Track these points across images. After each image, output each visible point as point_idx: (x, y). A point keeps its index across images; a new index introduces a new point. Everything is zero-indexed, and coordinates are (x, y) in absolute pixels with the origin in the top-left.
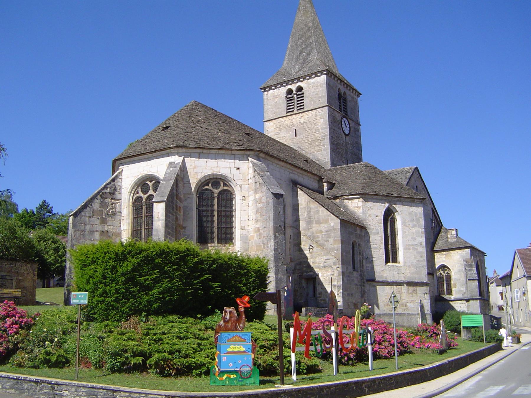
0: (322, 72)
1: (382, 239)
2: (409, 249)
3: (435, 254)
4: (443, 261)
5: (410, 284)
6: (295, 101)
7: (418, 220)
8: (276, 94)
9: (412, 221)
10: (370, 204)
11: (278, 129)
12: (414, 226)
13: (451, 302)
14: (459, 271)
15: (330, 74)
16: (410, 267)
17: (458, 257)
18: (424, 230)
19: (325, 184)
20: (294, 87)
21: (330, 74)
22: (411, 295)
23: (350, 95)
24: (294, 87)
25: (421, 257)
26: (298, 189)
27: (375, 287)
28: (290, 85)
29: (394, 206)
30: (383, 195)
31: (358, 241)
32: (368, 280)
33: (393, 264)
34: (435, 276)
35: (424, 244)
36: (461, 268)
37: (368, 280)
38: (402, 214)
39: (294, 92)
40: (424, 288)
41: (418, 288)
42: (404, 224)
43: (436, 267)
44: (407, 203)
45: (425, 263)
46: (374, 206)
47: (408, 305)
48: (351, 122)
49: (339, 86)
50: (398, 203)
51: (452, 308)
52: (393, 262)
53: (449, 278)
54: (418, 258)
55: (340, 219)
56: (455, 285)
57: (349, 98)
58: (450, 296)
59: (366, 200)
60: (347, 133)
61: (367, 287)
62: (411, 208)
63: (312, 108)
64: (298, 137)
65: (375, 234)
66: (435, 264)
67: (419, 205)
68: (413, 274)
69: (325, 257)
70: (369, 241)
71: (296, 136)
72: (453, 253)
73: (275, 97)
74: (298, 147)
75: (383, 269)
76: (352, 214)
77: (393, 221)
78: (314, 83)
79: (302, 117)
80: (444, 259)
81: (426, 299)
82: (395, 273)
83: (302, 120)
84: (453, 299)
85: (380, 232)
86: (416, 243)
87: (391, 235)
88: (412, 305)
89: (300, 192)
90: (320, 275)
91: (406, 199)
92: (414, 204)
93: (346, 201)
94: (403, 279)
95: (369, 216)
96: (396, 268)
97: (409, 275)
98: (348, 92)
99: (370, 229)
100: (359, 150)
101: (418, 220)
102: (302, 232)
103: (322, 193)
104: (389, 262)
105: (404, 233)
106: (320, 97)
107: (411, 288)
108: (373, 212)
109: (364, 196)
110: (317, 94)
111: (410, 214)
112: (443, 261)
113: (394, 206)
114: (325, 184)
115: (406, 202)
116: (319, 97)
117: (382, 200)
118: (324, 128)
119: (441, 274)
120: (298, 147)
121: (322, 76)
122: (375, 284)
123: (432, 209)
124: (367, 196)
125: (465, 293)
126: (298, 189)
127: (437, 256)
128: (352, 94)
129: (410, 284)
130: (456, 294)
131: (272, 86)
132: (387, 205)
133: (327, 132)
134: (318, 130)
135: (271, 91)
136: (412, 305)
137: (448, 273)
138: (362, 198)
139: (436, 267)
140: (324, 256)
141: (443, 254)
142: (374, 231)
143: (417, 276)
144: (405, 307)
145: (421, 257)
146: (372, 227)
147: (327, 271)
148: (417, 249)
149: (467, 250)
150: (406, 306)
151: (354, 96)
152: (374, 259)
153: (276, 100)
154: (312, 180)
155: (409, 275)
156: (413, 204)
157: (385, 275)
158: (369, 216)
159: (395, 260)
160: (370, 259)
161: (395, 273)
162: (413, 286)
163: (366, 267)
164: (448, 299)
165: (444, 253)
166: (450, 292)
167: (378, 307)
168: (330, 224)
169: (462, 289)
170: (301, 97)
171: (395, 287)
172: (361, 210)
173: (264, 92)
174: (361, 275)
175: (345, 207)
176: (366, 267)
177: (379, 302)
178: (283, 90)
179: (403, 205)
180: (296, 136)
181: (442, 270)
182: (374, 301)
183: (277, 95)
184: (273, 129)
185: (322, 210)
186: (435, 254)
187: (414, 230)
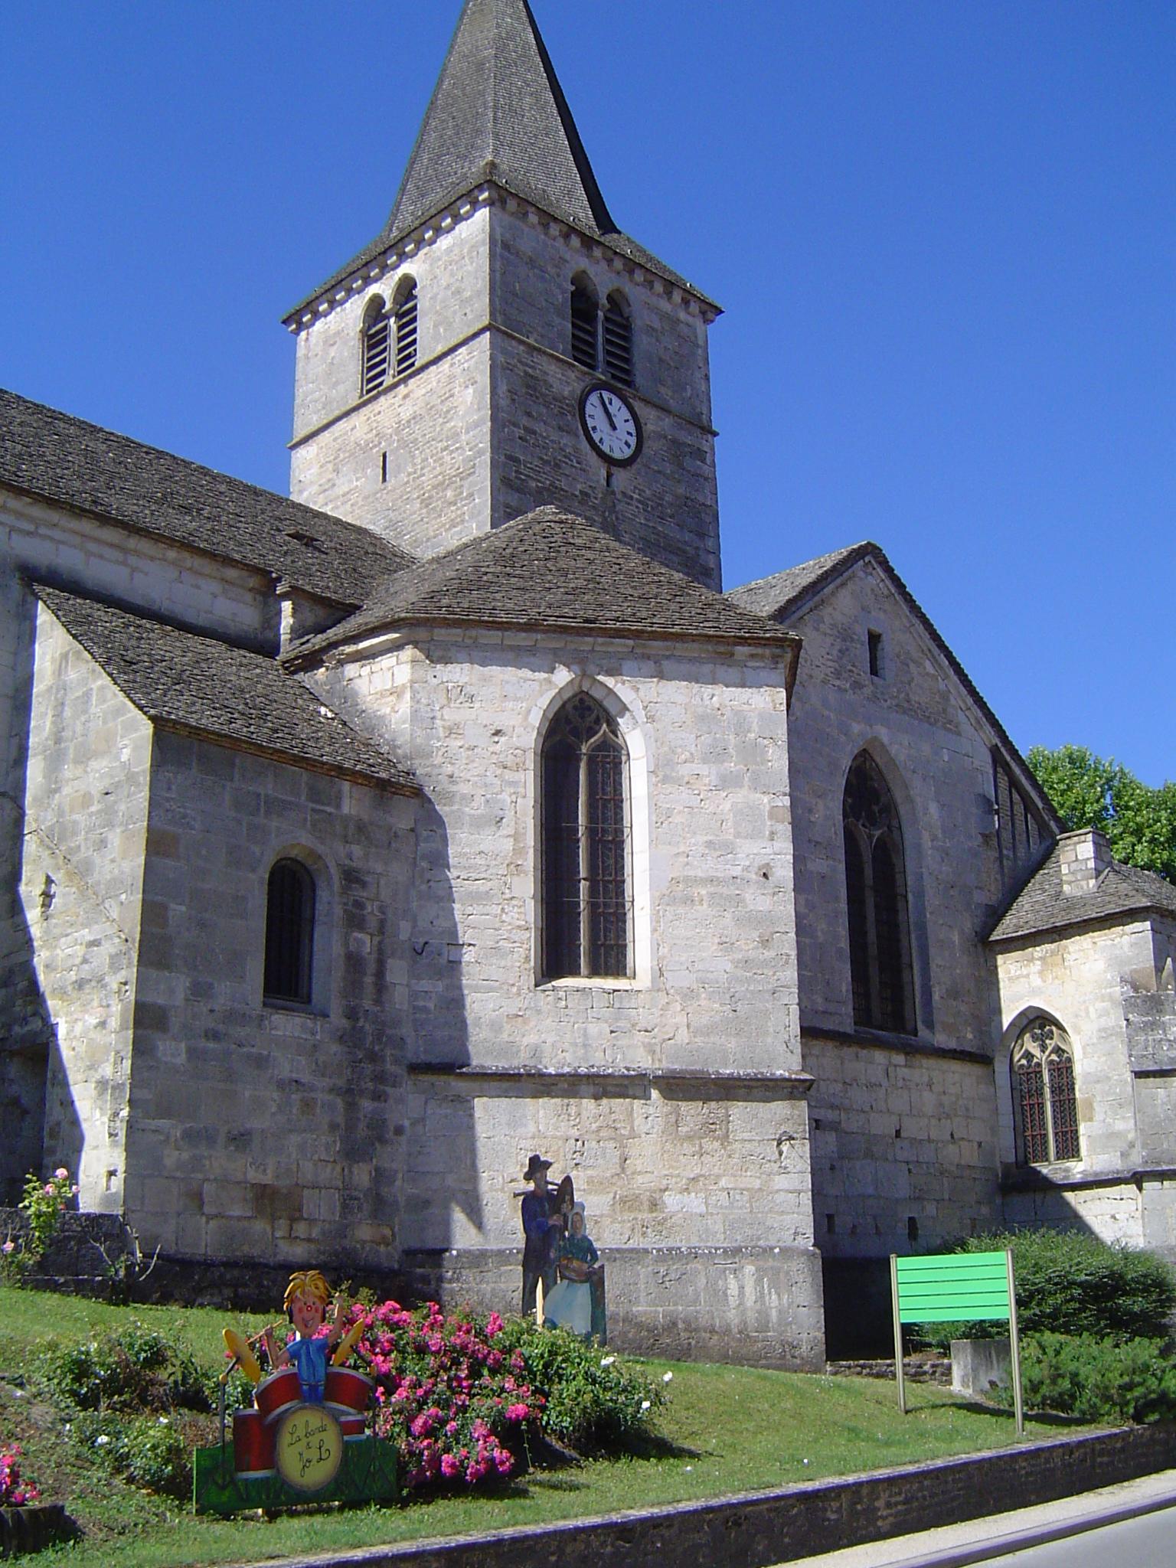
0: (470, 196)
1: (518, 851)
2: (689, 901)
3: (1000, 959)
4: (1034, 992)
5: (682, 1086)
6: (390, 345)
7: (752, 753)
8: (333, 328)
9: (716, 754)
10: (459, 673)
11: (330, 466)
12: (727, 783)
13: (1069, 1196)
14: (1106, 1034)
15: (503, 195)
16: (689, 995)
17: (1101, 965)
18: (786, 801)
19: (287, 606)
20: (385, 288)
21: (512, 205)
22: (688, 1148)
23: (645, 306)
24: (385, 288)
25: (765, 943)
26: (40, 603)
27: (464, 1104)
28: (376, 280)
29: (610, 681)
30: (531, 627)
31: (334, 854)
32: (417, 1068)
33: (598, 982)
34: (1001, 1067)
35: (784, 872)
36: (1111, 1022)
37: (417, 1068)
38: (651, 719)
39: (388, 306)
40: (780, 1109)
41: (739, 1111)
42: (662, 772)
43: (1007, 1020)
44: (685, 667)
45: (790, 975)
46: (485, 680)
47: (672, 1201)
48: (645, 412)
49: (582, 263)
50: (627, 665)
51: (1075, 1223)
52: (595, 972)
53: (1063, 1069)
54: (747, 944)
55: (152, 718)
56: (1090, 1105)
57: (641, 318)
58: (1071, 1164)
59: (437, 654)
60: (621, 452)
61: (409, 1103)
62: (708, 690)
63: (440, 349)
64: (390, 485)
65: (478, 823)
66: (998, 1011)
67: (763, 674)
68: (708, 1031)
69: (87, 935)
70: (439, 860)
71: (384, 480)
72: (1078, 946)
73: (329, 342)
74: (392, 525)
75: (512, 1007)
76: (374, 724)
77: (609, 763)
78: (449, 250)
79: (405, 397)
80: (1036, 981)
81: (785, 1171)
82: (593, 1029)
83: (406, 412)
84: (1078, 1178)
85: (509, 815)
86: (737, 871)
87: (592, 832)
88: (695, 1203)
89: (44, 616)
90: (62, 1032)
91: (680, 648)
92: (733, 673)
93: (351, 670)
94: (644, 1062)
95: (452, 731)
96: (600, 1002)
97: (683, 1036)
98: (636, 293)
99: (450, 797)
100: (702, 536)
101: (752, 753)
102: (30, 812)
103: (269, 649)
104: (574, 972)
105: (660, 817)
106: (469, 300)
107: (692, 1112)
108: (476, 717)
109: (422, 634)
110: (458, 292)
111: (706, 720)
112: (1034, 992)
113: (610, 681)
114: (287, 606)
115: (680, 659)
116: (463, 302)
117: (532, 650)
118: (476, 425)
119: (1028, 1055)
120: (392, 525)
121: (477, 214)
122: (459, 1086)
123: (994, 751)
124: (440, 634)
125: (1132, 1145)
126: (40, 603)
127: (1008, 966)
128: (665, 306)
129: (682, 1086)
130: (1092, 1151)
131: (317, 299)
132: (563, 676)
133: (481, 438)
134: (455, 435)
135: (319, 325)
136: (695, 1203)
137: (1058, 1050)
138: (416, 644)
139: (1007, 1020)
140: (84, 926)
141: (1032, 960)
142: (477, 808)
143: (732, 1044)
144: (646, 1216)
145: (765, 943)
146: (464, 789)
147: (85, 1007)
148: (738, 900)
149: (1137, 926)
150: (654, 1205)
151: (682, 315)
152: (468, 956)
153: (332, 352)
154: (215, 587)
155: (683, 1036)
156: (721, 671)
157: (532, 1039)
158: (452, 731)
159: (610, 959)
160: (440, 957)
161: (593, 1029)
162: (706, 1100)
163: (414, 995)
164: (1058, 1178)
165: (1038, 951)
166: (1069, 1148)
167: (478, 1222)
168: (117, 758)
169: (1120, 1126)
170: (407, 316)
171: (588, 1104)
172: (405, 706)
173: (297, 332)
174: (350, 1038)
175: (348, 697)
176: (414, 995)
177: (484, 1185)
178: (351, 314)
179: (661, 676)
180: (384, 480)
181: (1034, 1038)
182: (451, 1181)
183: (338, 333)
184: (315, 470)
185: (102, 688)
186: (1000, 959)
187: (726, 803)
